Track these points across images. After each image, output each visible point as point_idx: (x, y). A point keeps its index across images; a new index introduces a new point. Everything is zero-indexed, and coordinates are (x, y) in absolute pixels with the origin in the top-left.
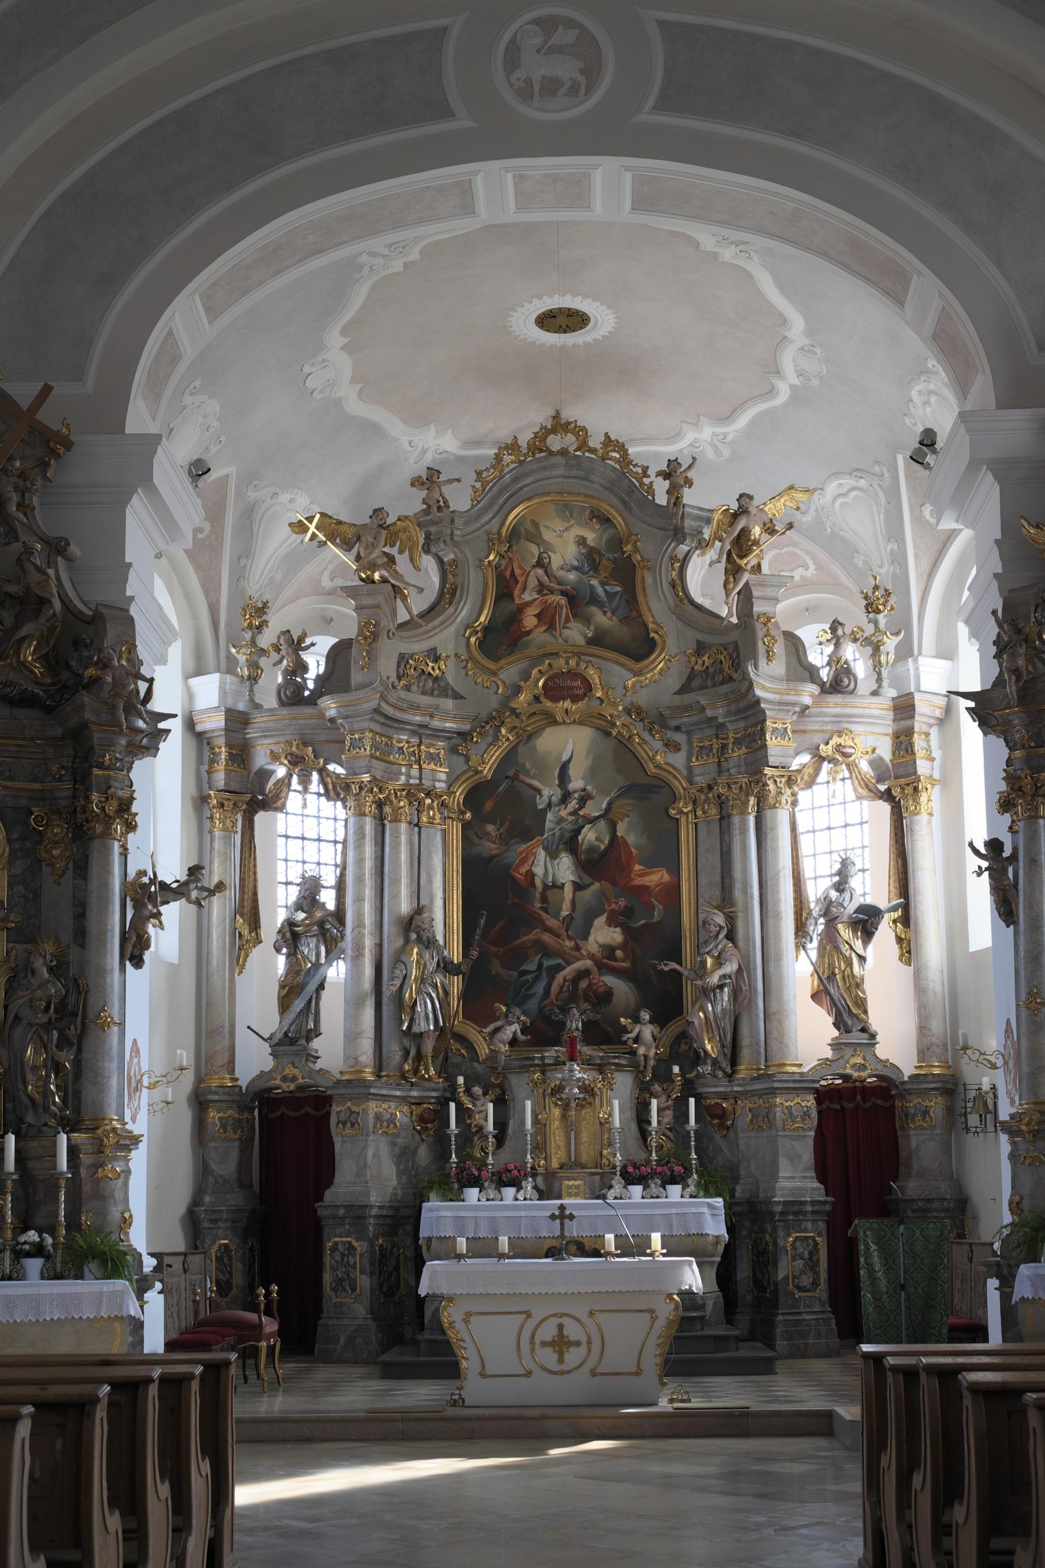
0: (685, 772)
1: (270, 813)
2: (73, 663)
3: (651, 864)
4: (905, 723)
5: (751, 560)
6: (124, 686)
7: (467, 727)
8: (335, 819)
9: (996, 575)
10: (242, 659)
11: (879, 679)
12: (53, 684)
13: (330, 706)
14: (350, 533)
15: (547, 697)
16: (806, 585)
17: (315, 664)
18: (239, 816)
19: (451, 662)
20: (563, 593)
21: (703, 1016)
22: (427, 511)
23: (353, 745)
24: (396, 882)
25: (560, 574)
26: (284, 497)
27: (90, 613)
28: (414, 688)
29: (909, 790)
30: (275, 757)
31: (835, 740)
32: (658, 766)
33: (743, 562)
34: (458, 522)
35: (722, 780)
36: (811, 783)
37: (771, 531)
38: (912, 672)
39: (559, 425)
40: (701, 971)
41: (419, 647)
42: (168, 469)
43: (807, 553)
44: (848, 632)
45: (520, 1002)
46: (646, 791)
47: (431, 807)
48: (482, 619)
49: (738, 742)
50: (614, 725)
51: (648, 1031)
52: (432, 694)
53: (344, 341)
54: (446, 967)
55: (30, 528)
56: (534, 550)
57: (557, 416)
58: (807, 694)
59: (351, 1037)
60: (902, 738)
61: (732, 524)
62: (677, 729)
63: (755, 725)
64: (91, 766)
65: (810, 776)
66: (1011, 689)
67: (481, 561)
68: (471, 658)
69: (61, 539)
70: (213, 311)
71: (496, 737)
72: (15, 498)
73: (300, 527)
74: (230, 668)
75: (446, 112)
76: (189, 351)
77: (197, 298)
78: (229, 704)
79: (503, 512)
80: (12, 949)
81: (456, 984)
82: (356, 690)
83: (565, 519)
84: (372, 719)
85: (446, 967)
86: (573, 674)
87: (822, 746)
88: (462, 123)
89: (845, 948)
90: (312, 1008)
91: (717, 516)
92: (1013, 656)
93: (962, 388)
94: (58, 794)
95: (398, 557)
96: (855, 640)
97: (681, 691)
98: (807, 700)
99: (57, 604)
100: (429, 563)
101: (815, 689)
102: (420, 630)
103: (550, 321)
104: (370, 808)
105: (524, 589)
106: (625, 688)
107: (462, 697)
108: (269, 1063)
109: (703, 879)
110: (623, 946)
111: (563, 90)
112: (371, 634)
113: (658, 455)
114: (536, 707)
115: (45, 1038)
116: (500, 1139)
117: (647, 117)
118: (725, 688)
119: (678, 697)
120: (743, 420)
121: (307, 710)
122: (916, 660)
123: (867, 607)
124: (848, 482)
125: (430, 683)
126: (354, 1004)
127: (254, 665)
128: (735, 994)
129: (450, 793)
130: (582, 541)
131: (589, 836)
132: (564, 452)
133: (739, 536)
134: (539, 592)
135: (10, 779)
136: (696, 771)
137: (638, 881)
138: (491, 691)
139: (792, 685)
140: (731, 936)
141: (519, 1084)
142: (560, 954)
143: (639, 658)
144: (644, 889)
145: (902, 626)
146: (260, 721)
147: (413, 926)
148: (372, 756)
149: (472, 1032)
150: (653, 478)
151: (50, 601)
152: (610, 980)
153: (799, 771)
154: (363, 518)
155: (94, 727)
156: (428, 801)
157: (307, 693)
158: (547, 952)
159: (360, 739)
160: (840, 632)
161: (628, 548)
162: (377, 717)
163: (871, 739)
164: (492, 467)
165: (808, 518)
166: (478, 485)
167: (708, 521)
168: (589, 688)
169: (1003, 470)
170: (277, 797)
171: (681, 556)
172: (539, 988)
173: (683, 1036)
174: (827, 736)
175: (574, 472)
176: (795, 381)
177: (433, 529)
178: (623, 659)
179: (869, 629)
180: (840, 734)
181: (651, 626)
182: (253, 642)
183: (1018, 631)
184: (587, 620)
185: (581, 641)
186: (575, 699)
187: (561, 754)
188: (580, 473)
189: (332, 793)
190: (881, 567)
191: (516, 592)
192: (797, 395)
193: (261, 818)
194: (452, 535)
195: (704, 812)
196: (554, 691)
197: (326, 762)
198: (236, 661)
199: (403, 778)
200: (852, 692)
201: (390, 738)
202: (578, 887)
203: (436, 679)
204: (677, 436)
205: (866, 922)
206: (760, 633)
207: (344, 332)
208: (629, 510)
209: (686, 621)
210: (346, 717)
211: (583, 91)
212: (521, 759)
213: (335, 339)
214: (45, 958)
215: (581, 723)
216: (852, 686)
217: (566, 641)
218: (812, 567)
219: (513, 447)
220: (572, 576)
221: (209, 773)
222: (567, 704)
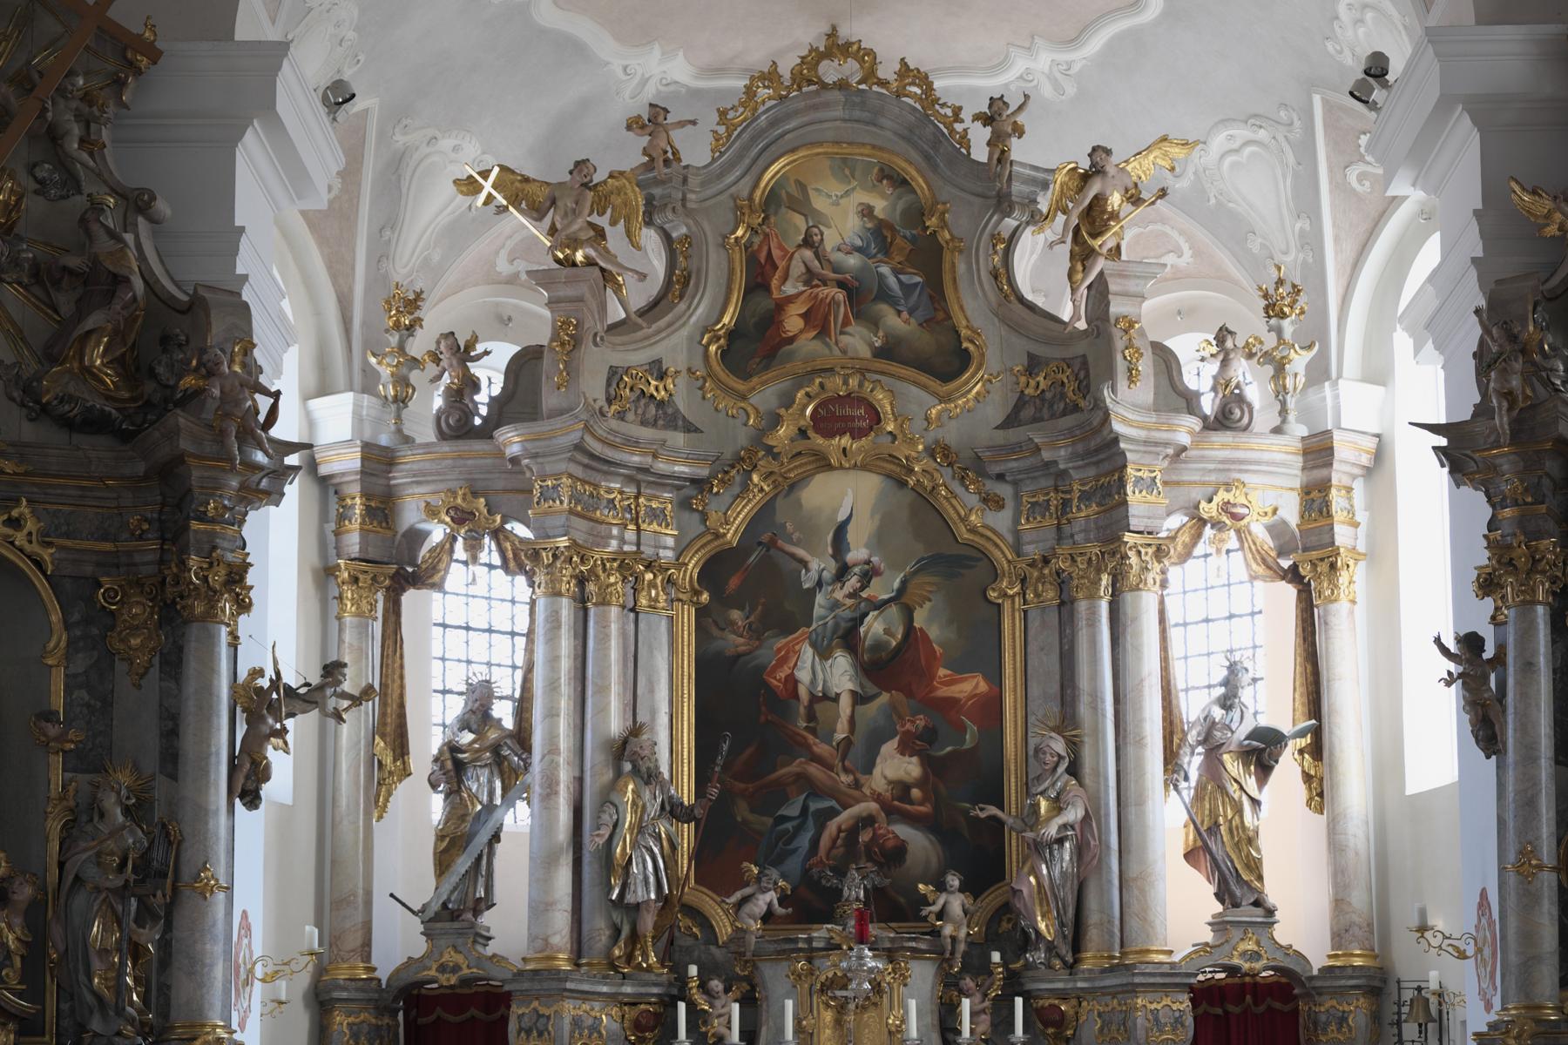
0: (1010, 538)
1: (424, 591)
2: (160, 370)
3: (962, 666)
4: (1319, 474)
5: (1107, 241)
6: (238, 403)
7: (704, 472)
8: (513, 602)
10: (385, 372)
11: (1283, 411)
12: (133, 399)
13: (511, 440)
14: (542, 195)
15: (817, 430)
17: (491, 376)
19: (682, 380)
20: (841, 284)
21: (1035, 882)
22: (649, 166)
24: (603, 690)
25: (837, 257)
26: (446, 143)
27: (185, 298)
28: (630, 416)
29: (1323, 567)
30: (432, 512)
31: (1222, 496)
32: (973, 530)
33: (1096, 243)
34: (694, 181)
36: (1186, 555)
37: (1135, 199)
40: (1032, 818)
41: (639, 358)
42: (295, 96)
43: (1182, 232)
45: (774, 857)
46: (956, 566)
47: (652, 585)
48: (726, 320)
49: (1085, 497)
50: (911, 471)
51: (957, 903)
52: (654, 424)
54: (673, 810)
56: (800, 222)
57: (832, 34)
59: (539, 909)
60: (1315, 494)
62: (1000, 477)
63: (1111, 473)
64: (188, 518)
65: (1185, 545)
66: (1502, 421)
67: (725, 237)
68: (711, 374)
69: (142, 191)
71: (746, 487)
72: (77, 130)
73: (469, 186)
74: (368, 384)
79: (761, 163)
80: (71, 781)
81: (687, 835)
84: (571, 460)
85: (673, 810)
86: (851, 399)
87: (1203, 504)
89: (1233, 789)
90: (482, 869)
94: (137, 558)
96: (1250, 356)
98: (1184, 439)
99: (138, 284)
102: (640, 334)
104: (567, 585)
105: (785, 278)
106: (927, 419)
107: (697, 430)
108: (419, 947)
109: (1034, 690)
110: (921, 783)
112: (570, 338)
113: (974, 91)
114: (801, 445)
115: (120, 908)
118: (1069, 421)
120: (1095, 44)
121: (479, 446)
122: (1335, 384)
123: (1266, 309)
124: (1242, 133)
125: (652, 409)
126: (543, 864)
127: (402, 381)
128: (1080, 851)
129: (680, 564)
130: (867, 212)
131: (874, 627)
132: (842, 85)
133: (1090, 206)
134: (807, 283)
135: (68, 536)
136: (1026, 538)
137: (944, 692)
138: (738, 422)
139: (1164, 417)
140: (1074, 770)
141: (775, 977)
142: (832, 793)
143: (947, 376)
144: (952, 702)
145: (1316, 337)
146: (410, 460)
147: (627, 752)
148: (571, 512)
149: (708, 903)
150: (968, 123)
151: (127, 280)
152: (903, 831)
155: (191, 461)
156: (649, 576)
157: (478, 421)
158: (815, 791)
159: (554, 487)
160: (1229, 344)
161: (932, 222)
162: (579, 457)
163: (1272, 495)
164: (742, 104)
168: (876, 418)
169: (1487, 112)
170: (434, 569)
171: (1006, 235)
172: (804, 841)
173: (1006, 909)
175: (857, 114)
177: (657, 191)
178: (924, 378)
179: (1270, 341)
180: (1228, 486)
181: (964, 332)
182: (401, 349)
184: (874, 323)
185: (865, 352)
186: (857, 434)
187: (836, 511)
188: (865, 115)
189: (512, 564)
190: (1286, 253)
191: (774, 282)
193: (410, 598)
194: (684, 199)
195: (1037, 595)
196: (829, 420)
197: (505, 520)
200: (1246, 429)
201: (596, 486)
202: (858, 699)
203: (661, 404)
204: (1002, 65)
205: (1262, 752)
206: (1119, 344)
208: (934, 167)
209: (1015, 327)
210: (535, 456)
212: (780, 517)
214: (119, 793)
215: (864, 467)
216: (1246, 420)
217: (844, 352)
218: (1187, 253)
219: (770, 76)
220: (853, 261)
221: (337, 534)
222: (845, 441)
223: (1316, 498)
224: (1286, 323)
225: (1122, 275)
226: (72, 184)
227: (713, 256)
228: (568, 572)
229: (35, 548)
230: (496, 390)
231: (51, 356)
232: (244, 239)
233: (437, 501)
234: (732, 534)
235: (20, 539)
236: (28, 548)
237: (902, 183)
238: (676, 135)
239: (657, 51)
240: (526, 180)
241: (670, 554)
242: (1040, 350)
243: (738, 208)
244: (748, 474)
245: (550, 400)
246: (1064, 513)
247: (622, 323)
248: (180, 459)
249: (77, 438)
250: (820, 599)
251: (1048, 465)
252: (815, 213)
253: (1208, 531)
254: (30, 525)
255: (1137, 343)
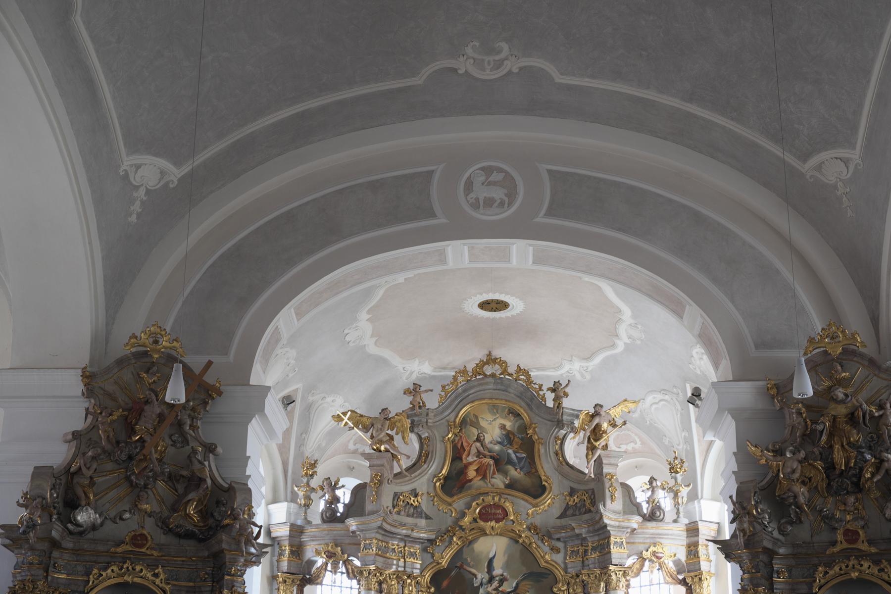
0: (562, 566)
1: (313, 586)
2: (216, 514)
4: (694, 539)
5: (602, 442)
6: (246, 530)
7: (433, 537)
8: (351, 588)
9: (734, 472)
10: (301, 494)
11: (678, 513)
12: (205, 526)
13: (352, 524)
15: (481, 518)
16: (635, 453)
17: (344, 496)
18: (295, 589)
19: (425, 497)
20: (491, 457)
22: (413, 408)
23: (365, 547)
25: (490, 446)
26: (329, 399)
27: (226, 486)
28: (402, 513)
29: (696, 579)
30: (318, 553)
31: (652, 549)
32: (547, 562)
33: (597, 444)
34: (431, 415)
35: (585, 571)
36: (637, 574)
37: (614, 425)
38: (697, 509)
39: (491, 360)
41: (407, 488)
42: (272, 404)
43: (636, 435)
44: (659, 484)
47: (410, 585)
48: (443, 472)
49: (594, 549)
50: (520, 536)
52: (413, 516)
53: (369, 316)
55: (196, 439)
56: (475, 431)
57: (489, 354)
58: (635, 521)
60: (692, 548)
61: (591, 421)
62: (558, 539)
63: (604, 539)
64: (224, 574)
65: (637, 569)
66: (741, 540)
67: (444, 437)
68: (437, 495)
69: (212, 444)
70: (299, 315)
71: (450, 543)
72: (189, 422)
73: (338, 418)
74: (293, 498)
75: (433, 215)
76: (285, 335)
77: (292, 310)
78: (292, 521)
79: (457, 410)
82: (369, 515)
83: (493, 414)
84: (377, 532)
86: (497, 506)
87: (644, 552)
88: (442, 220)
91: (582, 417)
92: (741, 523)
93: (716, 365)
94: (203, 589)
95: (395, 437)
96: (664, 489)
97: (561, 517)
98: (635, 526)
99: (209, 481)
100: (413, 437)
101: (640, 519)
102: (407, 479)
103: (485, 305)
104: (374, 586)
105: (468, 455)
106: (527, 514)
107: (430, 518)
111: (496, 204)
112: (378, 481)
113: (548, 377)
114: (474, 525)
116: (146, 347)
117: (541, 219)
118: (586, 517)
119: (559, 520)
120: (598, 360)
121: (339, 526)
122: (699, 502)
123: (670, 469)
124: (659, 396)
125: (412, 510)
127: (308, 497)
129: (422, 576)
130: (503, 427)
132: (493, 375)
133: (595, 428)
134: (477, 457)
135: (176, 580)
136: (569, 566)
138: (448, 515)
139: (626, 516)
143: (536, 496)
145: (691, 481)
146: (310, 531)
148: (376, 554)
150: (545, 391)
151: (205, 480)
153: (630, 568)
154: (375, 413)
155: (226, 552)
156: (409, 581)
157: (339, 514)
159: (370, 544)
160: (654, 484)
161: (530, 432)
162: (380, 531)
163: (673, 548)
164: (452, 383)
165: (636, 415)
166: (443, 394)
167: (577, 417)
168: (506, 514)
169: (737, 414)
170: (318, 576)
171: (561, 437)
174: (647, 546)
175: (499, 387)
176: (628, 341)
177: (416, 419)
178: (526, 497)
179: (672, 483)
180: (655, 545)
181: (543, 478)
182: (308, 484)
183: (744, 508)
184: (505, 473)
185: (502, 486)
187: (488, 553)
188: (503, 387)
189: (351, 575)
190: (678, 445)
191: (464, 456)
192: (628, 348)
193: (307, 589)
194: (427, 422)
195: (574, 590)
196: (485, 515)
197: (348, 556)
198: (297, 495)
199: (394, 567)
200: (661, 521)
201: (387, 543)
203: (416, 507)
204: (559, 367)
206: (607, 485)
207: (369, 312)
208: (531, 409)
209: (564, 475)
210: (362, 531)
211: (506, 205)
212: (465, 556)
213: (364, 316)
215: (501, 535)
216: (662, 517)
217: (493, 486)
218: (639, 443)
219: (463, 372)
220: (497, 448)
221: (278, 561)
222: (493, 523)
223: (692, 550)
224: (678, 475)
225: (608, 457)
226: (186, 442)
227: (438, 445)
228: (374, 580)
229: (163, 585)
230: (347, 501)
231: (174, 509)
232: (250, 461)
233: (320, 548)
234: (444, 563)
235: (158, 581)
236: (161, 585)
237: (517, 415)
238: (424, 396)
239: (417, 361)
240: (362, 416)
241: (418, 571)
242: (575, 486)
243: (449, 425)
244: (452, 537)
245: (369, 507)
246: (585, 555)
247: (400, 473)
248: (222, 551)
249: (183, 541)
250: (481, 591)
251: (578, 535)
252: (481, 428)
253: (647, 563)
254: (162, 576)
255: (614, 485)
